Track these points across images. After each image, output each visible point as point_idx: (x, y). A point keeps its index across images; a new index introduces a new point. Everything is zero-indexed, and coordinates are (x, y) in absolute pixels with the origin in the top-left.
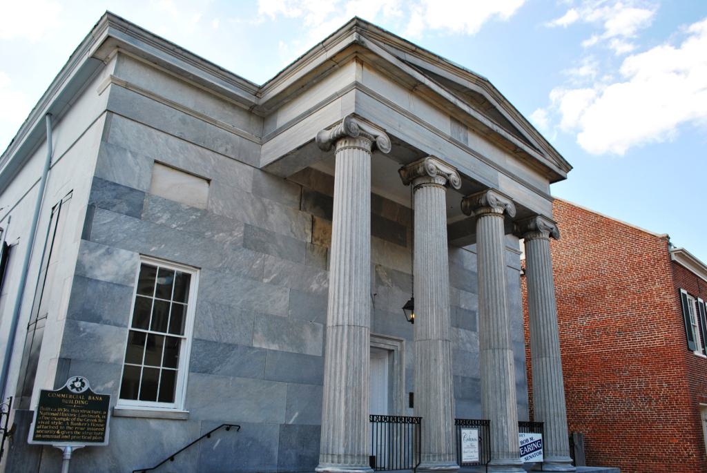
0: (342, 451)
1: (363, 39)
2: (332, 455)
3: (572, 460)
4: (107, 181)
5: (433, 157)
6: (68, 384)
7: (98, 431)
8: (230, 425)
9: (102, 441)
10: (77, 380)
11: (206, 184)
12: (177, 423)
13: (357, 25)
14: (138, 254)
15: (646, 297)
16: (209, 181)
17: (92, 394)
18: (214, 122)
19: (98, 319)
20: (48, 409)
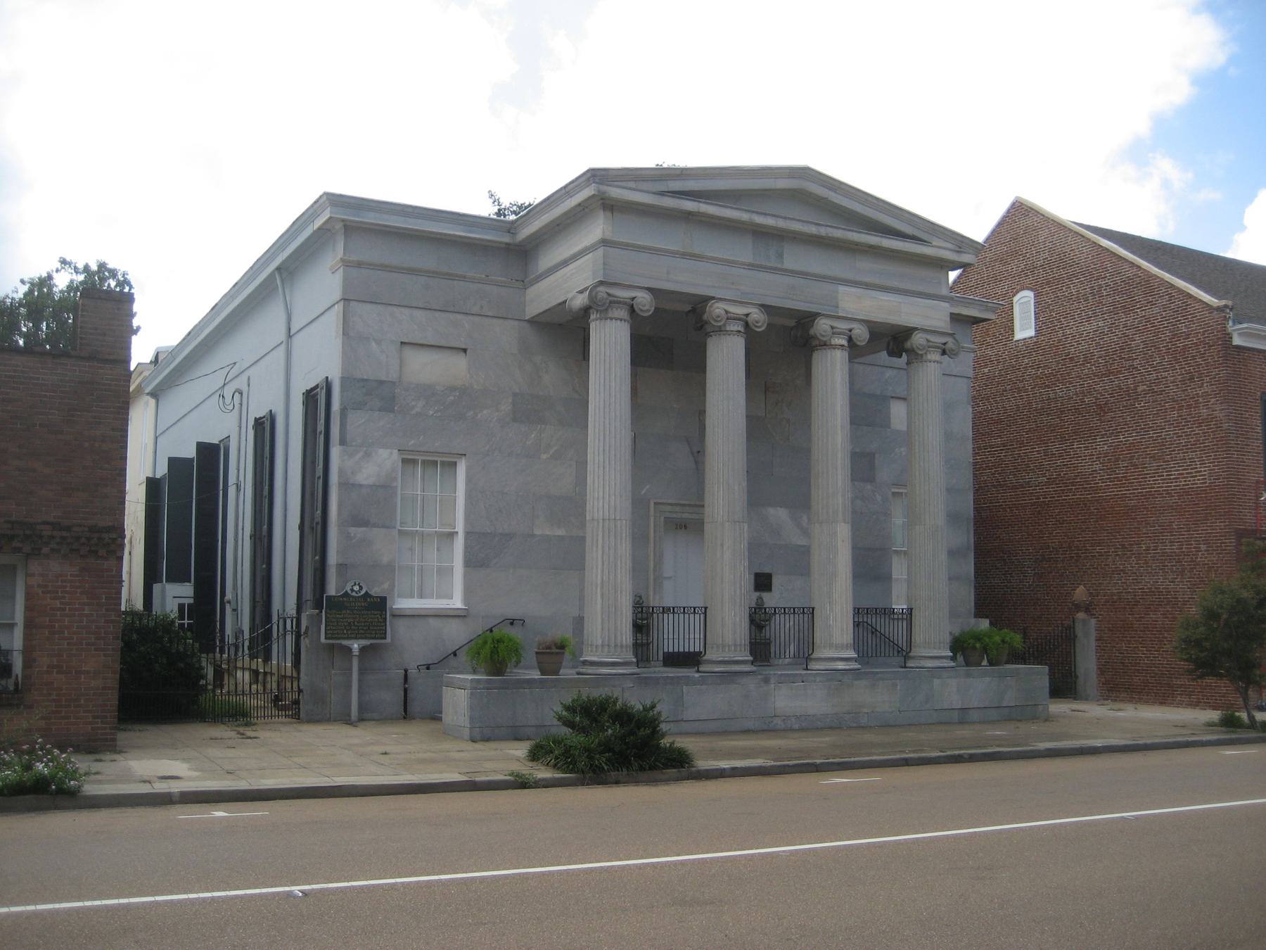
0: (600, 642)
1: (604, 188)
2: (608, 646)
3: (951, 654)
4: (355, 379)
5: (720, 299)
6: (348, 588)
7: (380, 630)
8: (514, 620)
9: (385, 638)
10: (355, 584)
11: (462, 354)
12: (457, 620)
13: (594, 176)
14: (397, 450)
15: (1189, 407)
16: (465, 350)
17: (371, 596)
18: (463, 278)
19: (366, 523)
20: (334, 611)
